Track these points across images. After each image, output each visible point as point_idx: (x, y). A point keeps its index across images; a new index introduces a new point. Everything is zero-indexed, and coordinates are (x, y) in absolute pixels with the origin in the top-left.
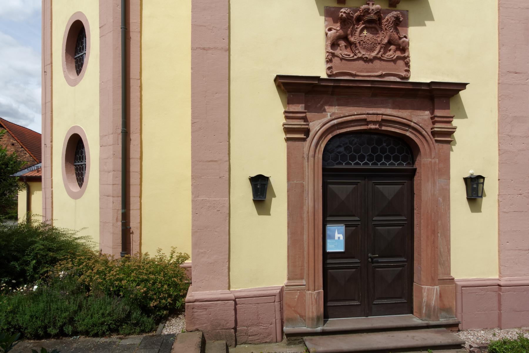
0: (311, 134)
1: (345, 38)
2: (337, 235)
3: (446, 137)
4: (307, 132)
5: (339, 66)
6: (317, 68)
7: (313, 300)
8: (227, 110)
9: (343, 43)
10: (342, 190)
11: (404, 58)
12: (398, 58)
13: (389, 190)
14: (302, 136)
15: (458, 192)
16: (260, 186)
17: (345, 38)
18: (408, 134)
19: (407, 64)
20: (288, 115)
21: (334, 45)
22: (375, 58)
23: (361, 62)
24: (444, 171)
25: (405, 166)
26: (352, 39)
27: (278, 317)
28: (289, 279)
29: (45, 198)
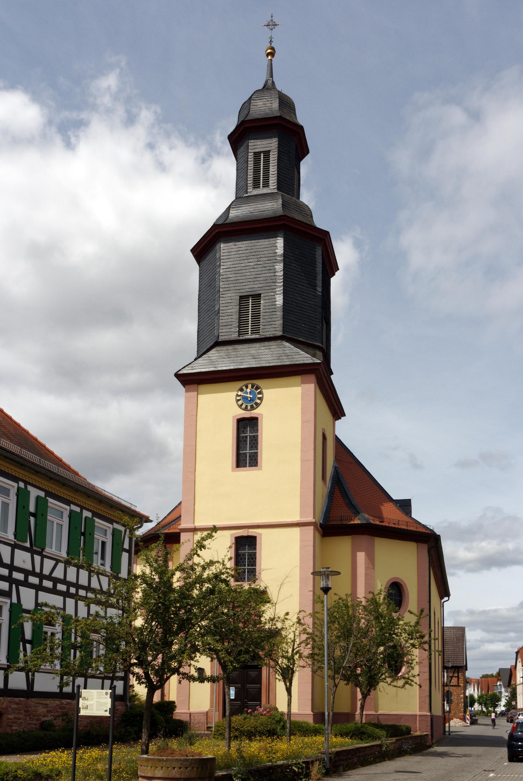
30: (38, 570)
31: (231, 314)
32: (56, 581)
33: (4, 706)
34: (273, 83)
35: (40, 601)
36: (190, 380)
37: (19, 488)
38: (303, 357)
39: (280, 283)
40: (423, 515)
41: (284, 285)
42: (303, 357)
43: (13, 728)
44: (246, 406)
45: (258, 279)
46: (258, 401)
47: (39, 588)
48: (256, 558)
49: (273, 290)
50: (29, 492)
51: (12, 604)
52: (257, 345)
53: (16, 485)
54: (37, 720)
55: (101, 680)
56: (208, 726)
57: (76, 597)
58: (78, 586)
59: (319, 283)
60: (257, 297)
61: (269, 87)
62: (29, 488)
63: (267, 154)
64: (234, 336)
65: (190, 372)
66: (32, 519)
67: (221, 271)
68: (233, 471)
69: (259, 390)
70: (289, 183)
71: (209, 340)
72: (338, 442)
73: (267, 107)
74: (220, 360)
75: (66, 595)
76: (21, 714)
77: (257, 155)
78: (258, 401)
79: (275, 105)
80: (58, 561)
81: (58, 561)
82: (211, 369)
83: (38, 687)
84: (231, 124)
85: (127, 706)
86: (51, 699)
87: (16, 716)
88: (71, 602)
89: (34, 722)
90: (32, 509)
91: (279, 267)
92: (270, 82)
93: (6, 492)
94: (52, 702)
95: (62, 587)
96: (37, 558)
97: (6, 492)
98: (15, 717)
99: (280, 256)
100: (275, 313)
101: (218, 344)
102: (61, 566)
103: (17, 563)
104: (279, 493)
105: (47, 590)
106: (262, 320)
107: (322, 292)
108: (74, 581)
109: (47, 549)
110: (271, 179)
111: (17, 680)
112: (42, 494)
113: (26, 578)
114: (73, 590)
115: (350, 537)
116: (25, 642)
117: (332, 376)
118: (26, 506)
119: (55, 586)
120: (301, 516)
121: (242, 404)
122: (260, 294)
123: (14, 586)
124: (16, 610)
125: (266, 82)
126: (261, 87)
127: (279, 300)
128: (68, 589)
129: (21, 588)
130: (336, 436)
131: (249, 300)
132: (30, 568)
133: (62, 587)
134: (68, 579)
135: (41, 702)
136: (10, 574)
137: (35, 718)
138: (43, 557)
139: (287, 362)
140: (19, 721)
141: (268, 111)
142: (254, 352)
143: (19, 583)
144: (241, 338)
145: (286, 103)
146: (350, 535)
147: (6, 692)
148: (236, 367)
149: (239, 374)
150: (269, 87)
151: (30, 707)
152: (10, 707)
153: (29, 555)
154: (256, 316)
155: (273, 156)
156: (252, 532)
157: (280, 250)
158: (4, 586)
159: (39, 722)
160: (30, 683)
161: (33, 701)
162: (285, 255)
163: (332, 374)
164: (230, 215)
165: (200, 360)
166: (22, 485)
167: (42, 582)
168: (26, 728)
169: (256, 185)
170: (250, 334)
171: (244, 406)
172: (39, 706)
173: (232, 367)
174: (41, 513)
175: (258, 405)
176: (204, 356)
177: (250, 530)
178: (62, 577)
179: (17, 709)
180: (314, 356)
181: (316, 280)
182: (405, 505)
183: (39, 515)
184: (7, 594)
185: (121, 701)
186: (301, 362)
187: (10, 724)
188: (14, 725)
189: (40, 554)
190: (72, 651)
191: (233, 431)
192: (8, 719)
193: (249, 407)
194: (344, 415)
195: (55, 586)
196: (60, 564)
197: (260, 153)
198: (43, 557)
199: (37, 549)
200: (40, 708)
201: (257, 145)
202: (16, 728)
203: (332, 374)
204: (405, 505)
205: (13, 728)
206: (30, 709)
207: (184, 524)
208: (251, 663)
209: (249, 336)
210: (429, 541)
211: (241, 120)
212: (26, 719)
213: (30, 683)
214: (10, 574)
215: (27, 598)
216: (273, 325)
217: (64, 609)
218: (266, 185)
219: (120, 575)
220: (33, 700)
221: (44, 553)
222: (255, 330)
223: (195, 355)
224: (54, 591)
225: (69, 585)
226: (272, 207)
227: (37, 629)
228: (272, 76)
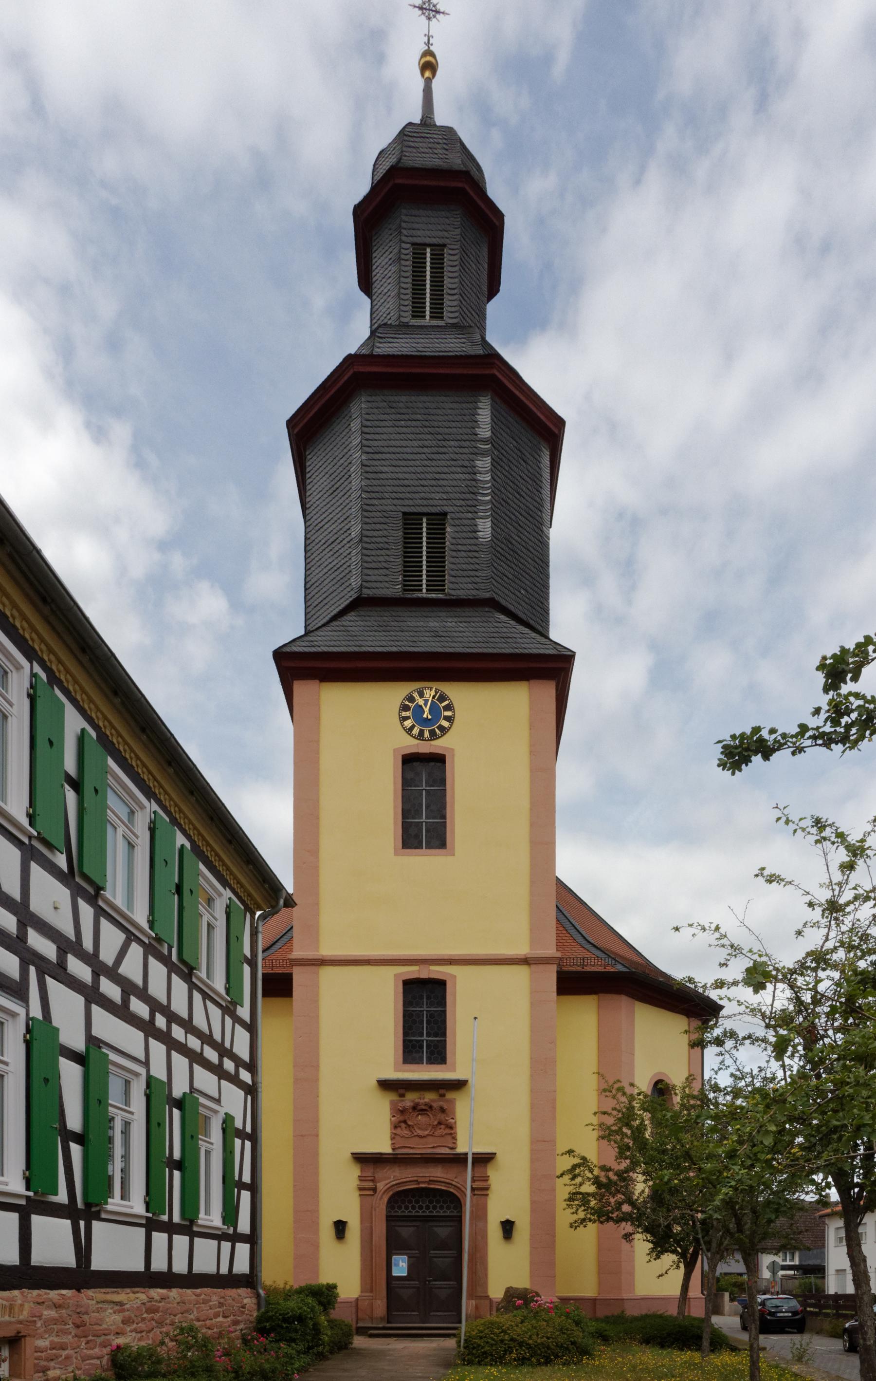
0: (378, 1191)
1: (405, 1122)
2: (401, 1264)
3: (482, 1190)
4: (375, 1190)
5: (400, 1142)
6: (384, 1147)
7: (380, 1307)
8: (187, 1122)
9: (403, 1125)
10: (406, 1232)
11: (451, 1134)
12: (447, 1134)
13: (443, 1231)
14: (371, 1193)
15: (494, 1231)
16: (340, 1228)
17: (405, 1122)
18: (451, 1190)
19: (455, 1138)
20: (361, 1178)
21: (396, 1127)
22: (428, 1135)
23: (417, 1139)
24: (480, 1214)
25: (455, 1214)
26: (410, 1123)
27: (354, 1316)
28: (362, 1292)
29: (112, 776)
30: (88, 944)
31: (387, 546)
33: (24, 1315)
43: (51, 1374)
44: (421, 733)
45: (441, 482)
46: (445, 724)
49: (473, 508)
54: (104, 1345)
55: (216, 1242)
56: (360, 1325)
60: (438, 520)
63: (439, 250)
68: (396, 854)
69: (447, 702)
74: (367, 635)
75: (148, 1028)
76: (66, 1333)
78: (445, 724)
83: (99, 1262)
85: (258, 1296)
86: (128, 1290)
87: (56, 1339)
89: (97, 1350)
94: (131, 1295)
98: (51, 1342)
100: (476, 554)
105: (106, 1004)
111: (53, 1241)
115: (595, 997)
120: (533, 943)
121: (413, 727)
122: (445, 514)
123: (32, 969)
124: (40, 1040)
135: (109, 1297)
137: (99, 1340)
140: (64, 1353)
142: (437, 624)
143: (45, 968)
144: (409, 595)
146: (595, 993)
147: (25, 1275)
151: (86, 1313)
152: (40, 1317)
155: (452, 258)
158: (4, 961)
159: (108, 1349)
160: (83, 1251)
161: (92, 1296)
168: (79, 1369)
170: (424, 591)
171: (416, 731)
172: (105, 1310)
177: (433, 968)
179: (55, 1321)
184: (19, 991)
185: (247, 1287)
187: (43, 1363)
188: (52, 1364)
191: (395, 777)
192: (38, 1350)
193: (427, 734)
200: (106, 1310)
202: (57, 1372)
205: (51, 1374)
206: (86, 1317)
207: (298, 953)
208: (438, 1212)
209: (424, 594)
212: (79, 1347)
213: (83, 1251)
215: (67, 1011)
217: (146, 1064)
220: (90, 1292)
222: (436, 583)
224: (122, 1012)
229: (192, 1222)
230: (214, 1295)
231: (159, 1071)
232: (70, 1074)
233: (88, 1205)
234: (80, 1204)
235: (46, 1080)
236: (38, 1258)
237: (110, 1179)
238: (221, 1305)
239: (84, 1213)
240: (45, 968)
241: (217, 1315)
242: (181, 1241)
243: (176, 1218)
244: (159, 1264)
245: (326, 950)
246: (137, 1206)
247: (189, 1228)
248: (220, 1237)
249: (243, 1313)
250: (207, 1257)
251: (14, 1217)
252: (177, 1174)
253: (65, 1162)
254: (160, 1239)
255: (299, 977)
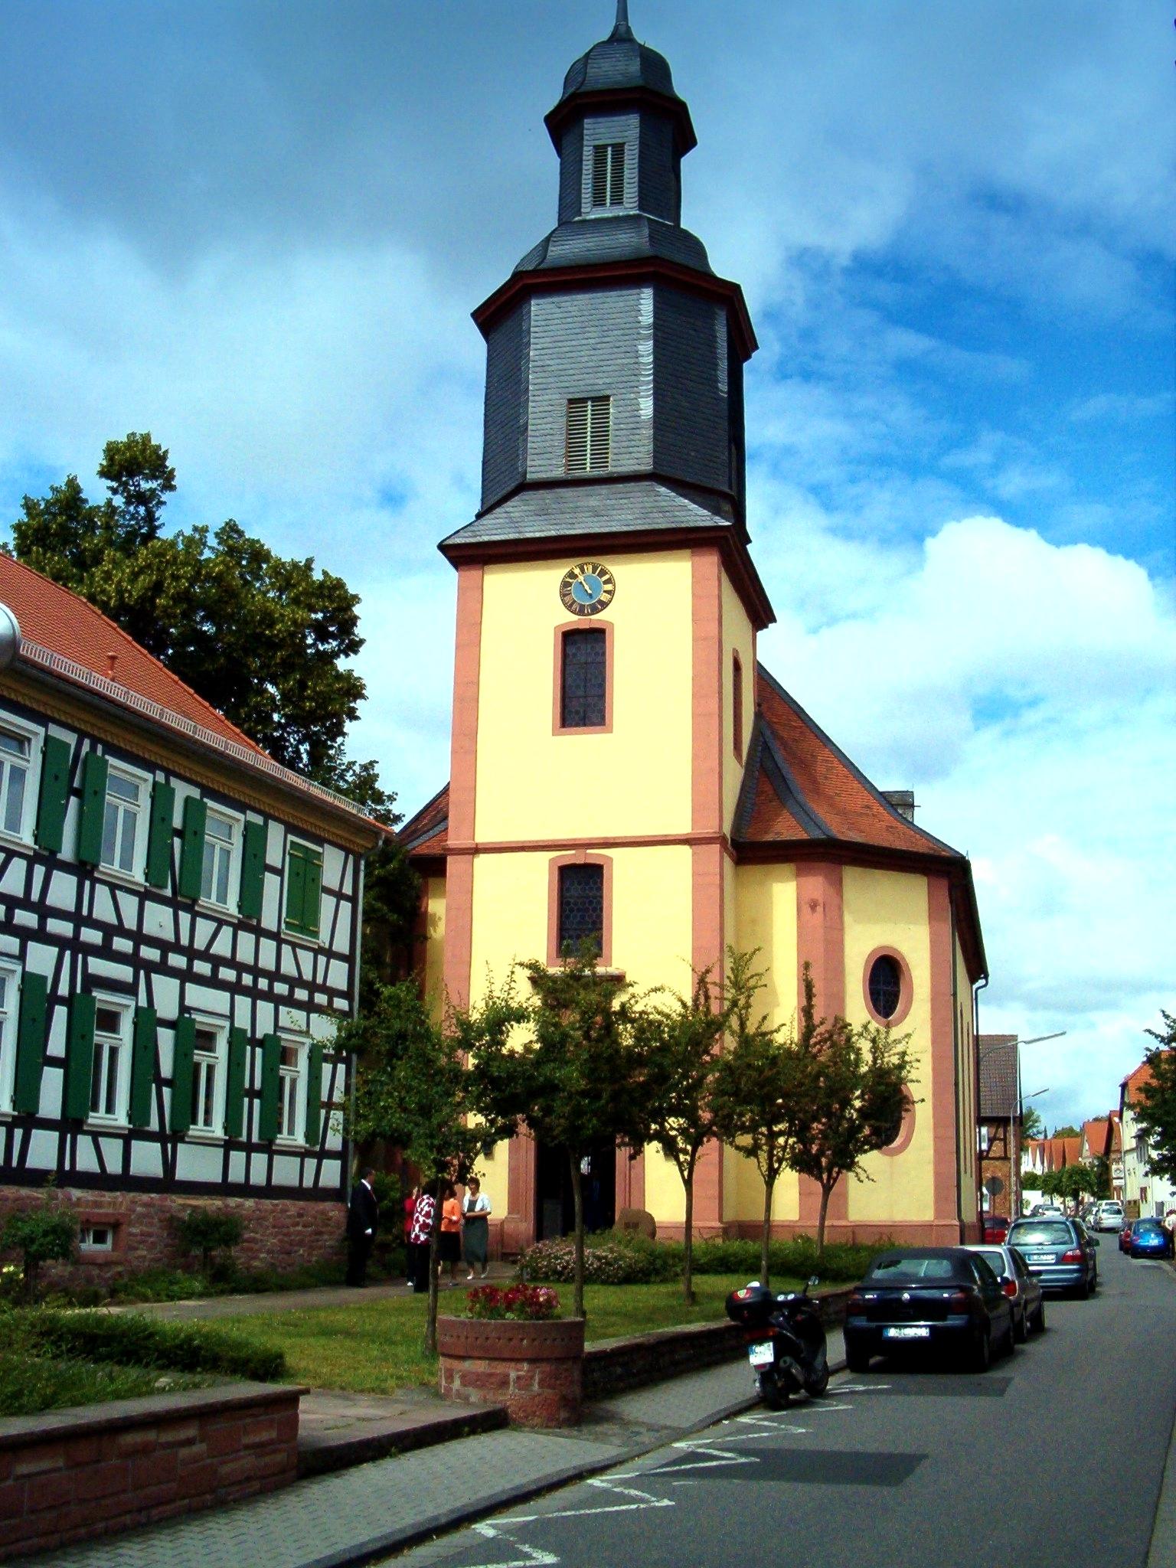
30: (184, 941)
32: (217, 962)
34: (628, 29)
35: (187, 1003)
36: (467, 556)
37: (155, 784)
38: (696, 515)
39: (647, 377)
40: (939, 819)
41: (654, 380)
42: (696, 515)
47: (186, 976)
48: (601, 909)
49: (634, 388)
50: (173, 790)
51: (138, 1009)
52: (604, 490)
53: (149, 776)
57: (254, 994)
58: (256, 971)
59: (723, 375)
61: (621, 37)
62: (175, 783)
63: (618, 149)
64: (559, 473)
65: (468, 540)
66: (177, 841)
67: (531, 353)
70: (662, 191)
71: (504, 480)
72: (764, 679)
73: (620, 70)
75: (235, 988)
77: (600, 151)
79: (635, 67)
80: (221, 923)
81: (221, 923)
82: (512, 536)
83: (182, 1173)
84: (552, 97)
88: (243, 1003)
90: (177, 822)
91: (646, 348)
92: (622, 29)
93: (20, 742)
95: (227, 974)
96: (185, 918)
97: (20, 742)
99: (647, 328)
101: (525, 486)
102: (227, 932)
103: (150, 928)
104: (646, 777)
106: (612, 444)
107: (729, 392)
108: (251, 962)
109: (203, 901)
110: (626, 191)
112: (196, 793)
113: (164, 957)
114: (247, 979)
116: (161, 1082)
117: (748, 547)
118: (167, 818)
119: (215, 971)
122: (607, 398)
123: (142, 973)
125: (616, 28)
126: (605, 37)
127: (646, 407)
128: (239, 977)
129: (154, 976)
130: (759, 664)
131: (587, 406)
132: (170, 936)
133: (227, 974)
134: (239, 957)
136: (136, 949)
138: (195, 915)
139: (662, 524)
141: (620, 78)
143: (151, 968)
145: (655, 65)
148: (562, 532)
149: (565, 545)
150: (621, 37)
153: (169, 911)
154: (601, 435)
156: (594, 855)
157: (647, 316)
162: (656, 326)
163: (749, 541)
164: (549, 253)
165: (488, 520)
166: (161, 777)
167: (193, 965)
169: (598, 201)
173: (553, 533)
174: (193, 832)
175: (604, 605)
176: (498, 510)
178: (227, 953)
180: (716, 511)
181: (715, 370)
182: (901, 803)
183: (189, 835)
186: (692, 525)
189: (190, 908)
190: (246, 1100)
194: (772, 619)
195: (215, 971)
196: (224, 928)
197: (605, 147)
198: (195, 915)
199: (184, 901)
201: (598, 131)
203: (749, 541)
204: (901, 803)
209: (588, 471)
210: (948, 876)
211: (571, 90)
213: (169, 1165)
214: (136, 949)
215: (166, 994)
216: (634, 451)
217: (231, 1017)
218: (617, 200)
219: (59, 856)
221: (96, 875)
223: (477, 507)
225: (241, 968)
226: (628, 242)
227: (182, 1055)
228: (626, 18)
229: (271, 1142)
230: (293, 1206)
231: (243, 1021)
232: (166, 1039)
233: (174, 1132)
234: (168, 1131)
235: (96, 793)
236: (134, 1170)
237: (944, 1319)
238: (300, 1215)
239: (171, 1137)
240: (151, 968)
241: (297, 1224)
242: (259, 1160)
243: (255, 1139)
244: (236, 1175)
245: (482, 837)
246: (218, 1130)
247: (267, 1147)
248: (303, 1155)
249: (328, 1225)
250: (286, 1171)
251: (120, 1142)
252: (257, 1102)
253: (64, 1026)
254: (238, 1157)
255: (453, 864)
